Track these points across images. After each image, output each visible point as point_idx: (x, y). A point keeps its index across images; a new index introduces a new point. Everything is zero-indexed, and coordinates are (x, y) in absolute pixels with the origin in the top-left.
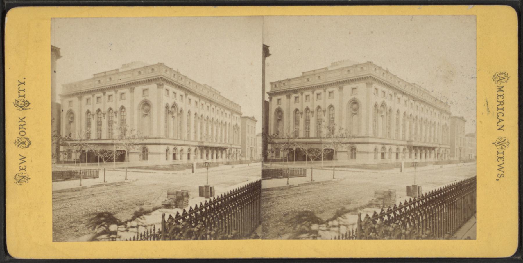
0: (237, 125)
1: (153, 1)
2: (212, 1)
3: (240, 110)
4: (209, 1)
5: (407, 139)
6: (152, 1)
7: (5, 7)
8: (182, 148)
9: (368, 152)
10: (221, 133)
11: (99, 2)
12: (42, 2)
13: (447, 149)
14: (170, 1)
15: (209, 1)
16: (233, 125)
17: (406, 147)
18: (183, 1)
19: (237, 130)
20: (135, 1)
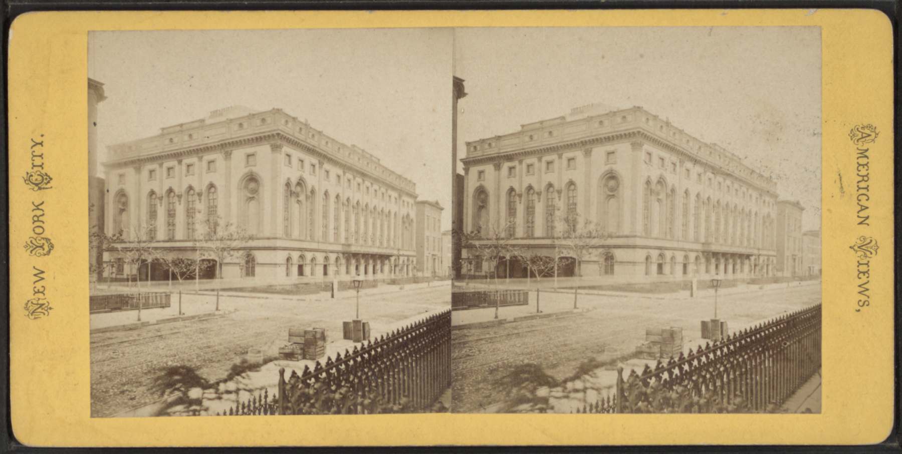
0: (408, 215)
1: (264, 2)
2: (366, 2)
3: (414, 189)
4: (361, 2)
5: (703, 240)
6: (261, 2)
7: (8, 12)
9: (634, 263)
10: (382, 229)
11: (171, 3)
12: (73, 3)
13: (771, 258)
14: (293, 2)
15: (361, 2)
17: (701, 254)
18: (316, 2)
19: (409, 224)
20: (233, 2)
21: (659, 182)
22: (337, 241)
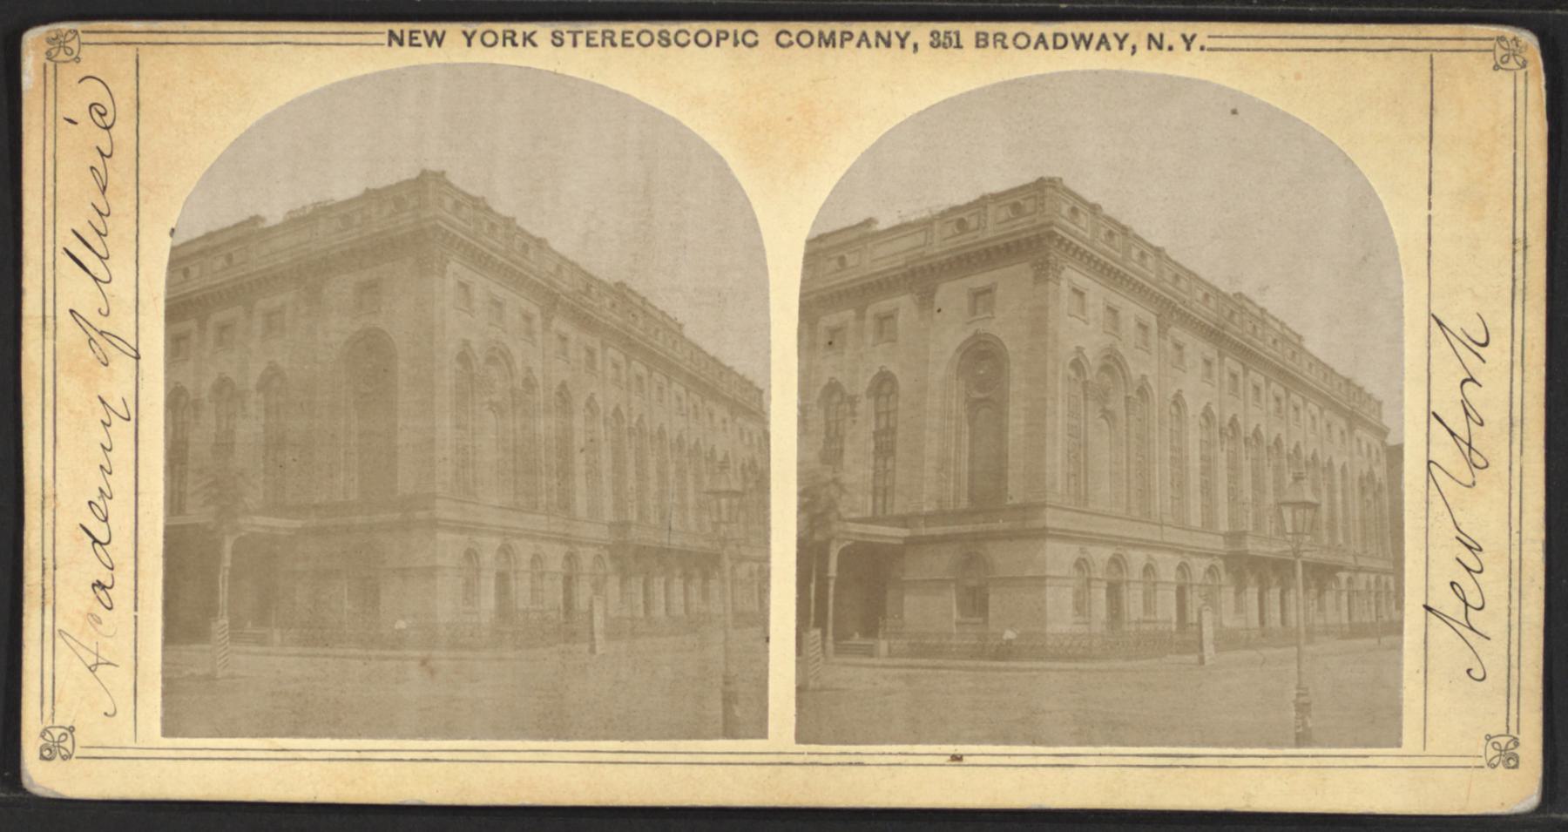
0: (1371, 474)
3: (1380, 415)
5: (1224, 527)
8: (1150, 558)
16: (1357, 476)
17: (1220, 563)
19: (1375, 495)
21: (1105, 368)
22: (1209, 525)
